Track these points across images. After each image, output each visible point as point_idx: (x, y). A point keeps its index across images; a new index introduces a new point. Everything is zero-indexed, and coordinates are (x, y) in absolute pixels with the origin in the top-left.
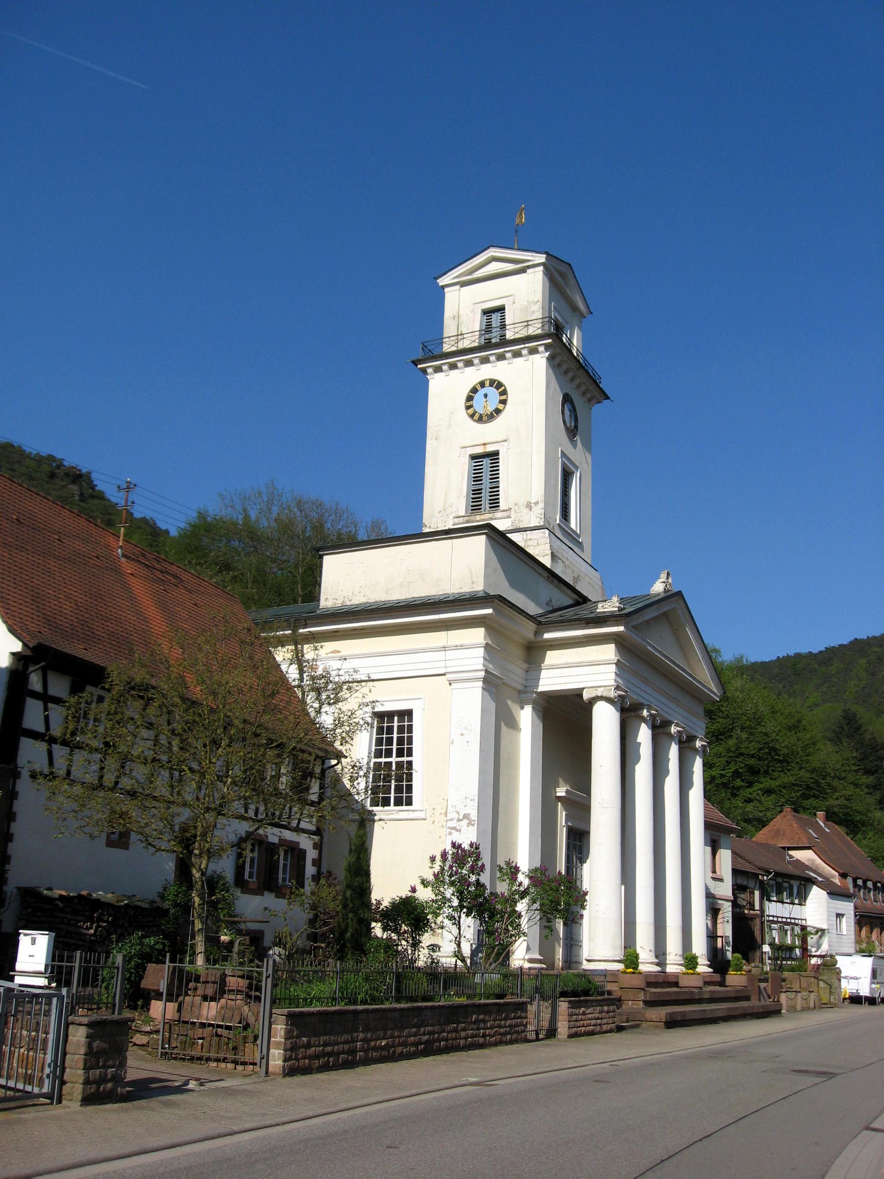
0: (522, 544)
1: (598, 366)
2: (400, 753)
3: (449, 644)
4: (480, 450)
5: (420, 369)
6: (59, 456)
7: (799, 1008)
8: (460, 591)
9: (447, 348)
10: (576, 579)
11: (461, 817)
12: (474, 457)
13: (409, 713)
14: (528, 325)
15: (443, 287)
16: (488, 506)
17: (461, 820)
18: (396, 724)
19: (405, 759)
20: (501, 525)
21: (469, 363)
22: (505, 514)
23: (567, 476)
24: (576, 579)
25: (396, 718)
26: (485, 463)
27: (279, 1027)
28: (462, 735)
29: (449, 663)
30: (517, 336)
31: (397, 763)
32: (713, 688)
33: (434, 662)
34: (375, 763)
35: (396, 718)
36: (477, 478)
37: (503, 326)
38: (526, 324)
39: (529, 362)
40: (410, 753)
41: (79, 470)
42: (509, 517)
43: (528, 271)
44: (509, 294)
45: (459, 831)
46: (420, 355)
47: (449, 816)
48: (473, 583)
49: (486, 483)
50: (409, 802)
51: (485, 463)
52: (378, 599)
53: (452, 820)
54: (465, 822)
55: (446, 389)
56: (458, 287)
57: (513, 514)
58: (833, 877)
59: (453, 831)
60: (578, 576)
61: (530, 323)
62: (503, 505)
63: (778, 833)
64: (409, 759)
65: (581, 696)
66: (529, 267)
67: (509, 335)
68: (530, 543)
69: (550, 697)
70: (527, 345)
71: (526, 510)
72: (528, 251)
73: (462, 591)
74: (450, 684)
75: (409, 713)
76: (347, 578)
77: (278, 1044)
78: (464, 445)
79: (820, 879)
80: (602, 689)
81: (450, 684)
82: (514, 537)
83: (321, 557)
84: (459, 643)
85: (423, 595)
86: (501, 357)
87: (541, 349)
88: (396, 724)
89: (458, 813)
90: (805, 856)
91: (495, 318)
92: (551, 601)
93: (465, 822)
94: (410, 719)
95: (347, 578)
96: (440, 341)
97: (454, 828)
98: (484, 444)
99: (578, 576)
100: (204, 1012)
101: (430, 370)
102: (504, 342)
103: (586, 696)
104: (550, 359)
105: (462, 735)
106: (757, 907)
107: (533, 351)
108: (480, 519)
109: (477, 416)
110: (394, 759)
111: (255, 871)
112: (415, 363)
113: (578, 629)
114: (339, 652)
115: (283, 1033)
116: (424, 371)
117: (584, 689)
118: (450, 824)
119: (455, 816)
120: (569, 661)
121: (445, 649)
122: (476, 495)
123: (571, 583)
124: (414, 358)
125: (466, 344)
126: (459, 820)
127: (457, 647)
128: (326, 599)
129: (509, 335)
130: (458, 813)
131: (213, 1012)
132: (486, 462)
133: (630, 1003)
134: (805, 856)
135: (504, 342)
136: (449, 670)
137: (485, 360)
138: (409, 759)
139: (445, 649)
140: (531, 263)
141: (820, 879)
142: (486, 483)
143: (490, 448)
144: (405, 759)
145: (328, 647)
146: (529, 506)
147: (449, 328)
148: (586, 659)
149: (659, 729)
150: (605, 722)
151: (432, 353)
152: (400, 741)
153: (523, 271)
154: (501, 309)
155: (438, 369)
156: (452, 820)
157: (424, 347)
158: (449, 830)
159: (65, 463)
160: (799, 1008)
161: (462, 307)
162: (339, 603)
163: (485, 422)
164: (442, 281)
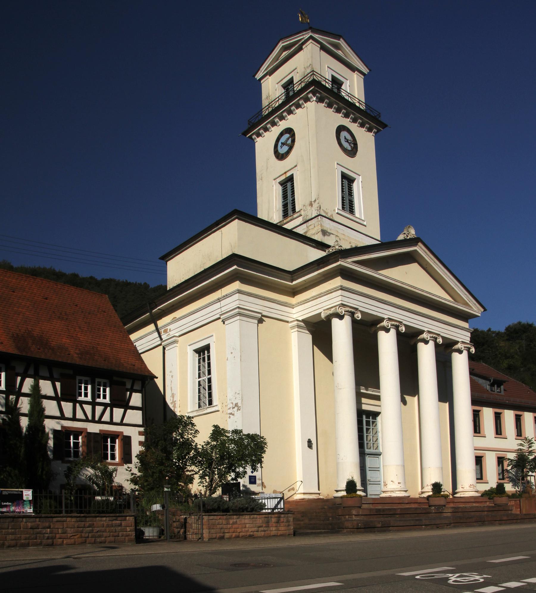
4: (283, 178)
7: (206, 539)
16: (291, 212)
26: (287, 184)
29: (223, 309)
42: (301, 215)
43: (304, 47)
44: (295, 68)
45: (233, 415)
51: (287, 184)
53: (230, 408)
55: (264, 144)
56: (268, 76)
57: (302, 213)
59: (231, 416)
62: (297, 210)
66: (303, 43)
71: (309, 208)
72: (366, 66)
74: (224, 323)
78: (275, 177)
81: (224, 323)
87: (310, 95)
89: (232, 403)
93: (236, 408)
97: (231, 414)
98: (285, 173)
103: (323, 316)
107: (307, 100)
111: (109, 452)
112: (245, 134)
116: (250, 137)
119: (231, 406)
124: (243, 131)
130: (232, 403)
133: (347, 517)
137: (282, 118)
139: (219, 300)
143: (288, 174)
153: (300, 49)
155: (259, 135)
158: (229, 415)
160: (206, 539)
161: (271, 89)
164: (258, 76)
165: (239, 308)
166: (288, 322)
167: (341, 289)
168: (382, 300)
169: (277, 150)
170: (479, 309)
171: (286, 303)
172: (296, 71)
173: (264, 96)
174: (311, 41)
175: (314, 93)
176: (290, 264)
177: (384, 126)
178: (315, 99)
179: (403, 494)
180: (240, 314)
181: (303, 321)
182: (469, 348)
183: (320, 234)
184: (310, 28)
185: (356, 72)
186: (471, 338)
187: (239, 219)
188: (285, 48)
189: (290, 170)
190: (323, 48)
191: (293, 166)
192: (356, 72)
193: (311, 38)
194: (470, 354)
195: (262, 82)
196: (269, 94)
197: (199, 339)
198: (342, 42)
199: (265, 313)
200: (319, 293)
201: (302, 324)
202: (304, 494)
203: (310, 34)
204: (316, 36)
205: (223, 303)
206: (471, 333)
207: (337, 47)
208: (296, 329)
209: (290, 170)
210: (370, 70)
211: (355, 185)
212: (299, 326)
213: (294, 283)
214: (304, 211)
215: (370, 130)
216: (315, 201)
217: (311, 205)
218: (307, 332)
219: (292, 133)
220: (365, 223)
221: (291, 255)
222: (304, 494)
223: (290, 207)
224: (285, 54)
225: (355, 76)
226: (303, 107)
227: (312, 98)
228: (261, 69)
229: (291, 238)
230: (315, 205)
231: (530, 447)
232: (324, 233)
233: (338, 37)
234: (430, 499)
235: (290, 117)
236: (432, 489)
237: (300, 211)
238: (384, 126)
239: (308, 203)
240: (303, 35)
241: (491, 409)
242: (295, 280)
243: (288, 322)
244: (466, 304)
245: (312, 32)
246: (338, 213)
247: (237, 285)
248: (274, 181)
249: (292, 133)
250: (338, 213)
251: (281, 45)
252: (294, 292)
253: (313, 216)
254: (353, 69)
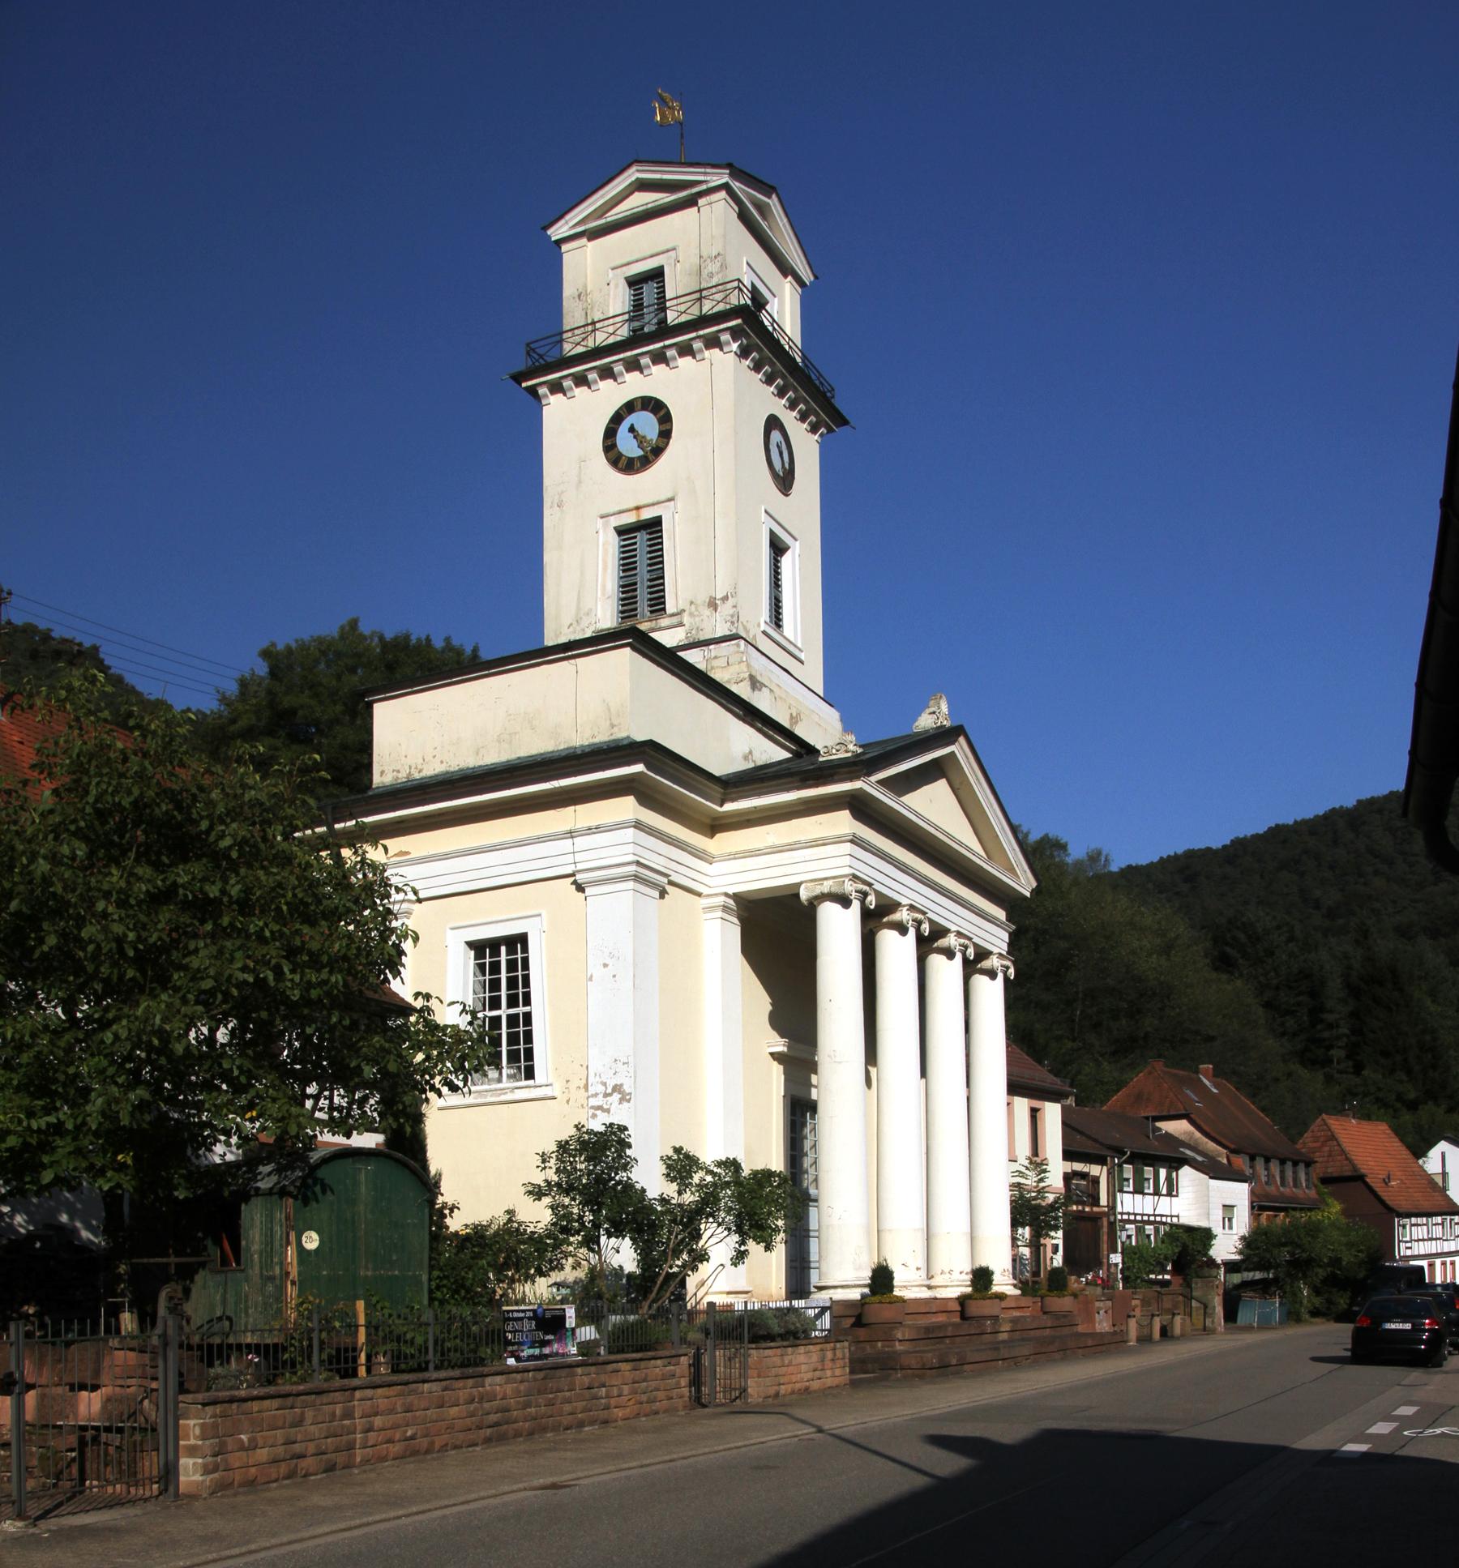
0: (701, 666)
1: (831, 373)
2: (513, 1002)
3: (578, 826)
4: (630, 519)
5: (527, 389)
6: (42, 626)
8: (592, 741)
9: (570, 349)
10: (794, 719)
11: (609, 1091)
12: (621, 531)
13: (522, 939)
14: (700, 299)
15: (559, 243)
16: (647, 609)
17: (610, 1095)
18: (503, 958)
19: (521, 1010)
20: (668, 638)
21: (607, 373)
22: (675, 620)
23: (778, 548)
24: (794, 719)
25: (503, 949)
26: (642, 539)
27: (192, 1422)
28: (605, 965)
29: (578, 857)
30: (684, 318)
31: (509, 1017)
32: (1024, 883)
33: (559, 856)
34: (1422, 1268)
35: (503, 949)
36: (627, 565)
37: (662, 308)
38: (697, 295)
39: (706, 363)
40: (527, 1001)
41: (80, 644)
42: (681, 625)
43: (701, 202)
44: (669, 246)
45: (608, 1111)
46: (521, 365)
47: (592, 1090)
48: (612, 726)
49: (643, 573)
50: (530, 1074)
51: (642, 539)
52: (463, 765)
53: (596, 1095)
54: (616, 1097)
55: (572, 420)
56: (584, 241)
57: (686, 619)
58: (1219, 1155)
59: (599, 1112)
60: (799, 714)
61: (704, 293)
62: (670, 607)
63: (1139, 1098)
64: (527, 1009)
65: (797, 895)
67: (672, 317)
68: (715, 663)
69: (750, 902)
70: (701, 333)
71: (707, 612)
73: (596, 740)
75: (522, 939)
76: (410, 733)
77: (192, 1451)
79: (1200, 1159)
80: (830, 882)
82: (686, 655)
83: (370, 706)
84: (594, 824)
85: (534, 752)
86: (659, 358)
87: (725, 337)
88: (503, 958)
89: (605, 1084)
90: (1178, 1128)
91: (649, 291)
92: (751, 752)
93: (616, 1097)
94: (525, 949)
95: (410, 733)
96: (558, 337)
98: (638, 508)
99: (799, 714)
100: (82, 1409)
101: (542, 391)
102: (665, 330)
103: (804, 895)
104: (744, 353)
105: (605, 965)
106: (1103, 1201)
107: (713, 342)
108: (629, 623)
109: (623, 462)
110: (503, 1012)
112: (518, 378)
113: (788, 790)
114: (407, 853)
115: (197, 1431)
116: (533, 391)
117: (800, 884)
118: (593, 1102)
120: (777, 843)
121: (571, 834)
122: (628, 592)
123: (786, 724)
125: (601, 339)
126: (606, 1095)
127: (599, 829)
128: (382, 773)
129: (672, 317)
130: (605, 1084)
131: (96, 1407)
132: (641, 538)
134: (1178, 1128)
135: (665, 330)
136: (580, 867)
137: (633, 365)
138: (527, 1009)
139: (571, 834)
140: (704, 187)
141: (1200, 1159)
142: (643, 573)
143: (647, 514)
144: (521, 1010)
145: (395, 844)
146: (713, 604)
147: (573, 315)
148: (803, 838)
149: (929, 942)
150: (838, 931)
151: (547, 361)
152: (512, 983)
153: (691, 202)
154: (657, 275)
155: (557, 388)
156: (596, 1095)
157: (530, 351)
158: (591, 1112)
159: (53, 634)
161: (593, 279)
162: (402, 777)
163: (638, 471)
164: (557, 232)
165: (638, 863)
166: (699, 895)
167: (852, 841)
168: (904, 864)
169: (614, 446)
170: (1029, 882)
171: (704, 852)
172: (672, 254)
173: (568, 290)
174: (723, 194)
175: (736, 333)
176: (720, 765)
177: (843, 421)
178: (735, 346)
179: (925, 1294)
180: (637, 878)
181: (736, 897)
182: (1008, 968)
183: (746, 685)
184: (729, 166)
185: (790, 278)
186: (1009, 945)
187: (634, 649)
188: (643, 186)
189: (653, 504)
190: (744, 217)
191: (663, 498)
192: (790, 278)
193: (726, 187)
194: (1006, 979)
195: (564, 248)
196: (585, 286)
197: (495, 920)
198: (773, 203)
199: (675, 878)
200: (790, 841)
201: (731, 902)
202: (729, 1293)
203: (725, 179)
204: (736, 186)
205: (581, 842)
206: (1010, 934)
207: (762, 209)
208: (720, 914)
209: (653, 504)
210: (816, 277)
211: (786, 561)
212: (725, 909)
213: (729, 807)
214: (691, 614)
215: (814, 429)
216: (725, 598)
217: (713, 604)
218: (736, 921)
219: (662, 413)
220: (802, 656)
221: (728, 746)
222: (729, 1293)
223: (642, 595)
224: (641, 200)
225: (788, 287)
226: (698, 357)
227: (728, 343)
228: (568, 217)
229: (708, 696)
230: (725, 610)
231: (1042, 1180)
232: (755, 684)
233: (768, 189)
234: (968, 1302)
235: (658, 370)
236: (972, 1281)
237: (679, 613)
238: (843, 421)
239: (703, 598)
240: (705, 174)
241: (1025, 1100)
242: (733, 800)
243: (699, 895)
244: (1012, 870)
245: (731, 175)
246: (764, 632)
247: (626, 807)
248: (600, 521)
249: (662, 413)
250: (764, 632)
251: (633, 174)
252: (714, 826)
253: (719, 634)
254: (785, 269)
